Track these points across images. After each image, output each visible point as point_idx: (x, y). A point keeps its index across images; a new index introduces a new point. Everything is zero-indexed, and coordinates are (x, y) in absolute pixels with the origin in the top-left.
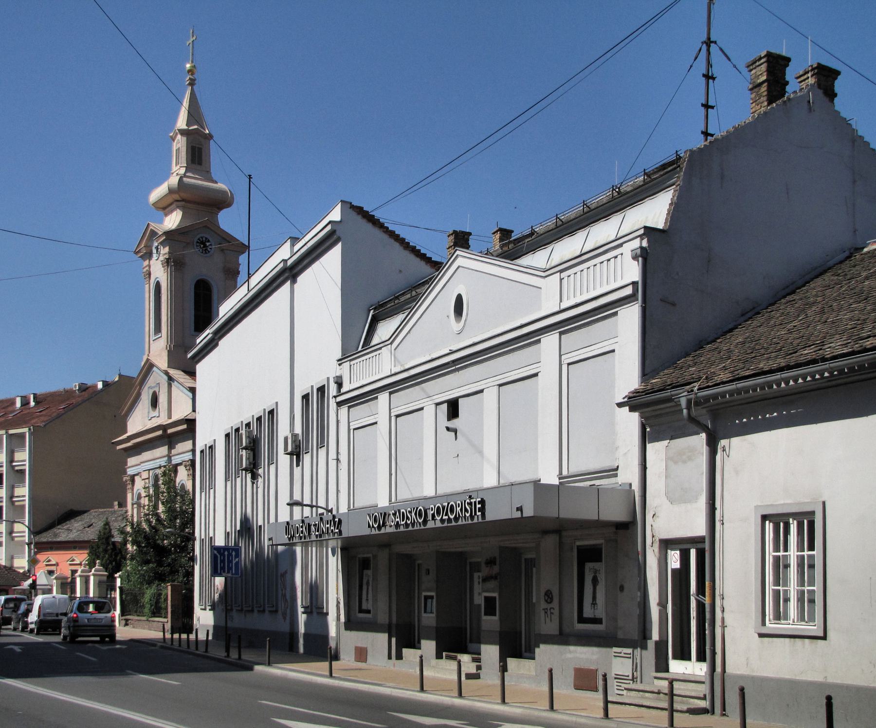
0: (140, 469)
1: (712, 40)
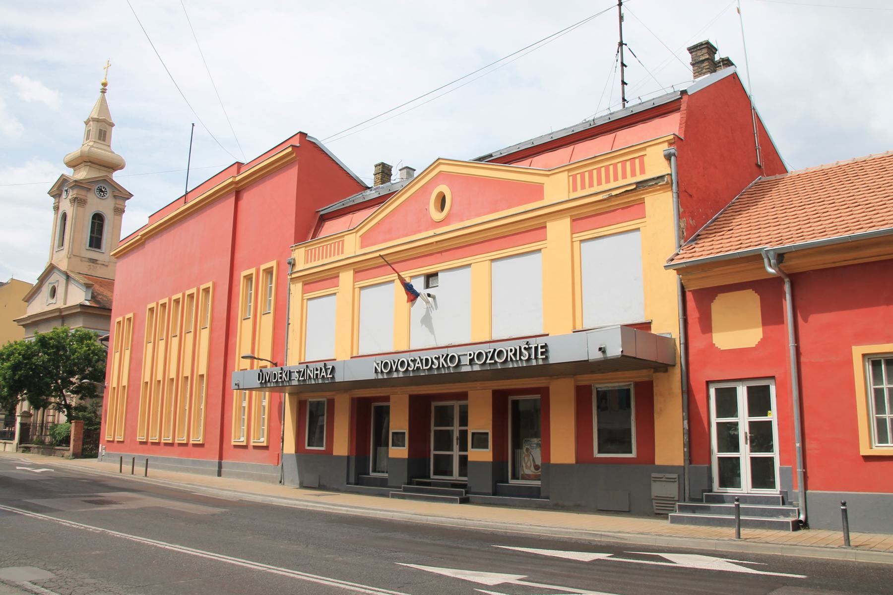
1: (623, 43)
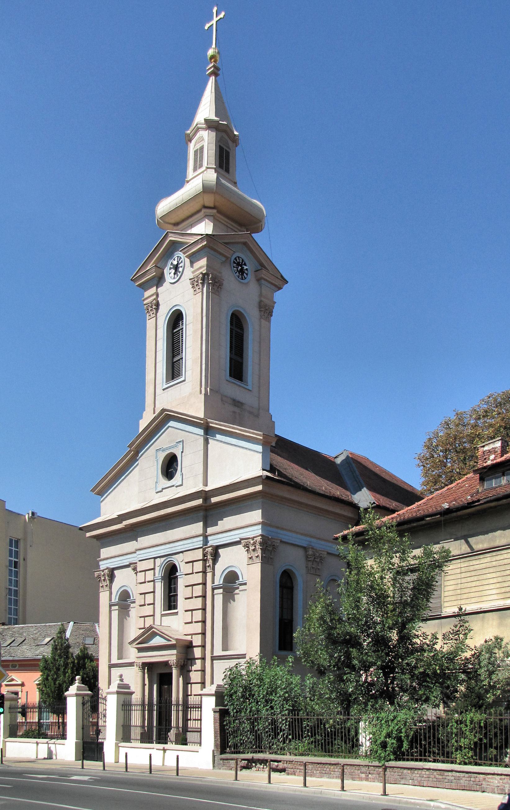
0: (136, 559)
